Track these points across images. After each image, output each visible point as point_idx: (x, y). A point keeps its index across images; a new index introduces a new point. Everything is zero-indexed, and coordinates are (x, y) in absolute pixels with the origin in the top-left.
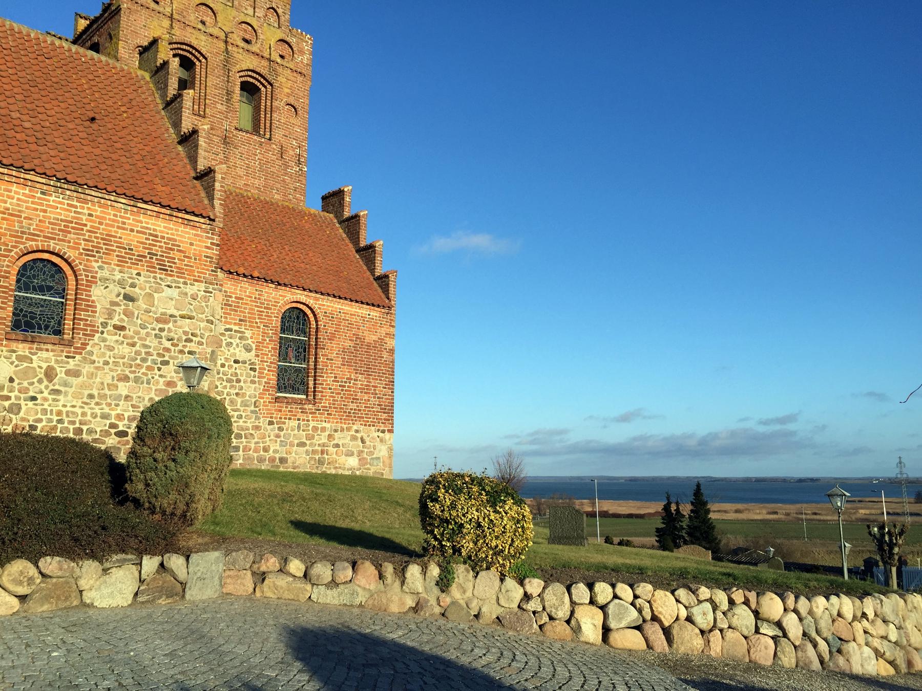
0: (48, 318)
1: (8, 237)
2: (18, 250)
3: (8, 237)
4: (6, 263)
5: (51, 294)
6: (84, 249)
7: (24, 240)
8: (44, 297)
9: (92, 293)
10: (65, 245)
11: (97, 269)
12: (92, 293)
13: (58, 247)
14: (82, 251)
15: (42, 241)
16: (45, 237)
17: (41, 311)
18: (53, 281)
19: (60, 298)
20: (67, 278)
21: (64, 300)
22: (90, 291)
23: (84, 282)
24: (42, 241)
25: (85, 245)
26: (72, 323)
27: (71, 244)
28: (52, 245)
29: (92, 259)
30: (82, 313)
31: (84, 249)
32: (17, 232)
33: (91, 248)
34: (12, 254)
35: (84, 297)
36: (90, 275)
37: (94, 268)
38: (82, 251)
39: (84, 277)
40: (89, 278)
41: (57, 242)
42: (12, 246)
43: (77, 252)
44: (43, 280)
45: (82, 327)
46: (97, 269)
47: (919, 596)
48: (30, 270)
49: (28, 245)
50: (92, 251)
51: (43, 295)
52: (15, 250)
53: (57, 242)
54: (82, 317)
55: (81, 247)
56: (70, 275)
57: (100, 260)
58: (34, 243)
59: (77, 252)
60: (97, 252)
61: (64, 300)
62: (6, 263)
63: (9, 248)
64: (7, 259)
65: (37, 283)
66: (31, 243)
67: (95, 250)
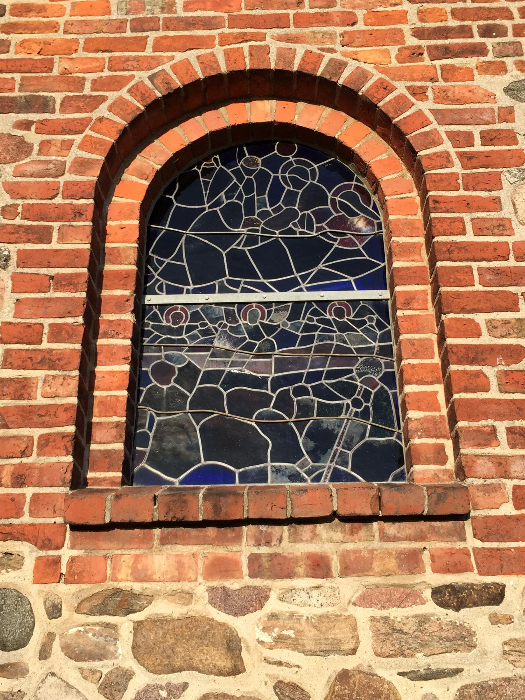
0: (319, 391)
1: (81, 54)
2: (124, 93)
3: (81, 54)
4: (75, 153)
5: (321, 275)
6: (418, 33)
7: (149, 52)
8: (291, 296)
9: (507, 212)
10: (332, 36)
11: (505, 101)
12: (507, 212)
13: (300, 50)
14: (412, 41)
15: (224, 40)
16: (234, 22)
17: (281, 364)
18: (322, 216)
19: (362, 285)
20: (375, 183)
21: (385, 294)
22: (496, 203)
23: (457, 168)
24: (224, 40)
25: (422, 16)
26: (440, 388)
27: (360, 26)
28: (274, 46)
29: (472, 62)
30: (481, 318)
31: (418, 33)
32: (120, 26)
33: (453, 23)
34: (102, 111)
35: (470, 237)
36: (476, 131)
37: (491, 97)
38: (412, 41)
39: (447, 146)
40: (478, 147)
41: (292, 30)
42: (96, 85)
43: (394, 50)
44: (274, 224)
45: (494, 394)
46: (505, 101)
47: (2, 663)
48: (214, 193)
49: (167, 67)
50: (465, 32)
51: (283, 287)
52: (112, 96)
53: (292, 30)
54: (486, 339)
55: (406, 29)
56: (389, 168)
57: (509, 61)
58: (191, 55)
59: (394, 50)
60: (486, 32)
61: (385, 294)
62: (75, 153)
63: (87, 91)
64: (78, 138)
65: (251, 240)
66: (179, 56)
67: (474, 25)
